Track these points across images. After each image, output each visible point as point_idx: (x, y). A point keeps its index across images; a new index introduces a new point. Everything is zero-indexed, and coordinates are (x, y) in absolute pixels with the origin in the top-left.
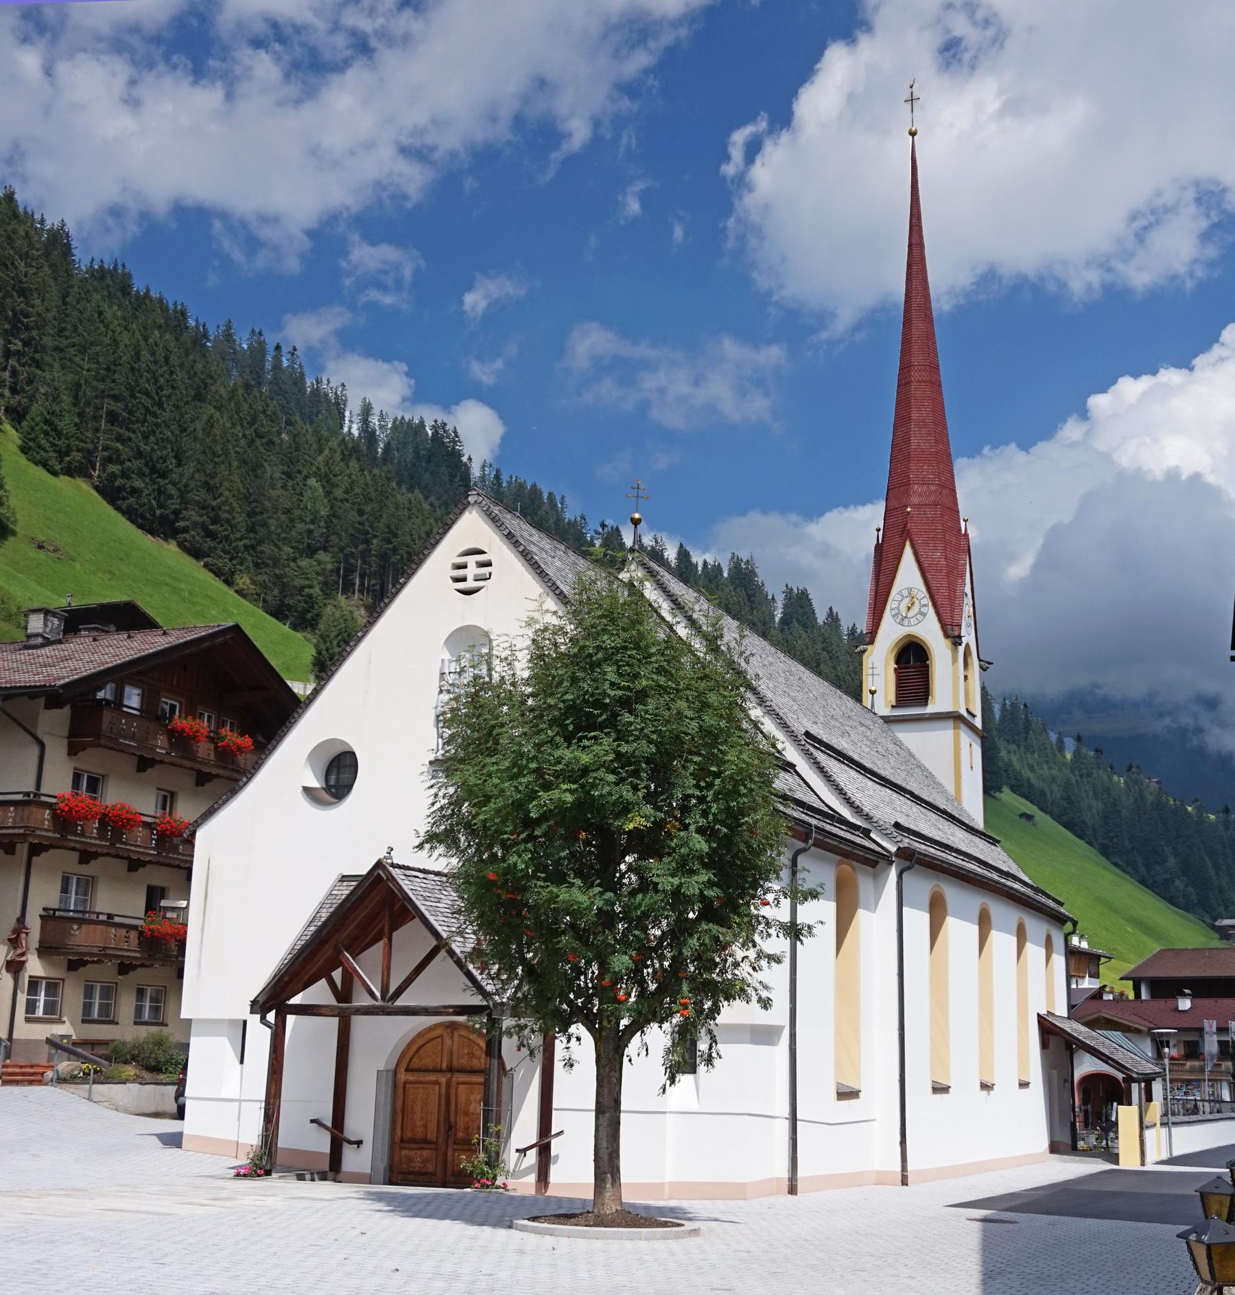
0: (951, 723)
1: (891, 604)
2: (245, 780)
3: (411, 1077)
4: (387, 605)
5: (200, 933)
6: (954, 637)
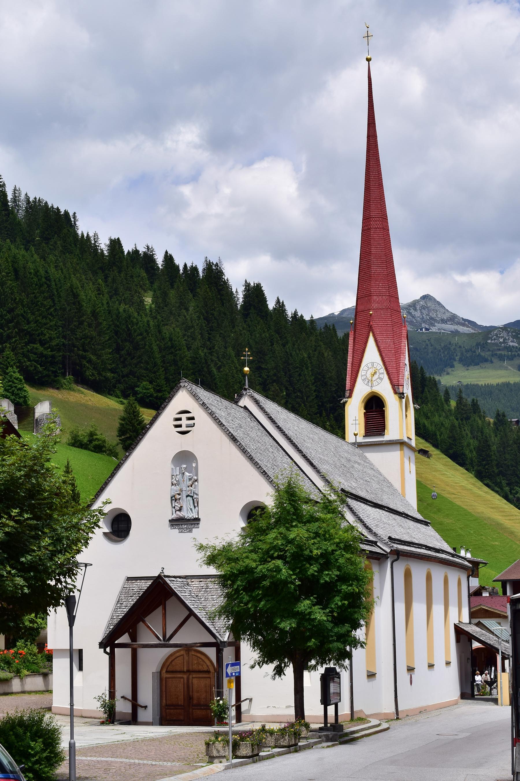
0: (398, 447)
1: (361, 372)
4: (141, 439)
6: (400, 394)
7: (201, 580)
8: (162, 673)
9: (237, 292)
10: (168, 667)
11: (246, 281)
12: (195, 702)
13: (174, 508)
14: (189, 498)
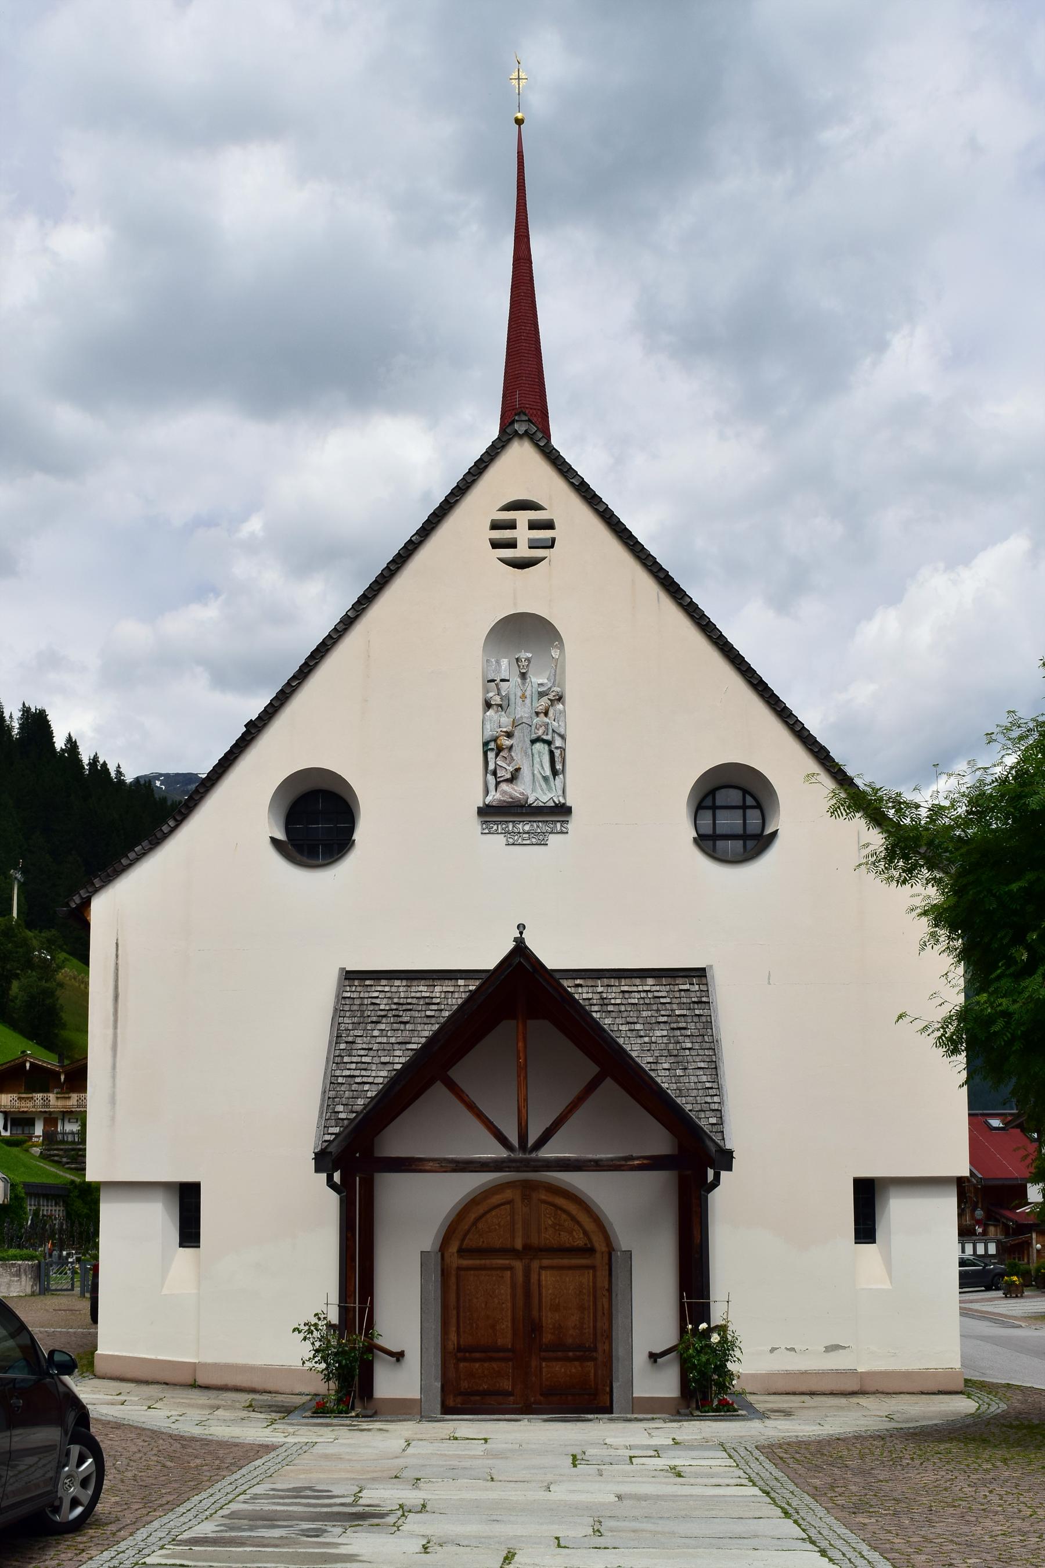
2: (172, 823)
3: (465, 1263)
5: (110, 1053)
7: (578, 982)
8: (446, 1255)
9: (11, 717)
10: (465, 1235)
11: (24, 704)
12: (547, 1338)
13: (494, 773)
14: (538, 746)
